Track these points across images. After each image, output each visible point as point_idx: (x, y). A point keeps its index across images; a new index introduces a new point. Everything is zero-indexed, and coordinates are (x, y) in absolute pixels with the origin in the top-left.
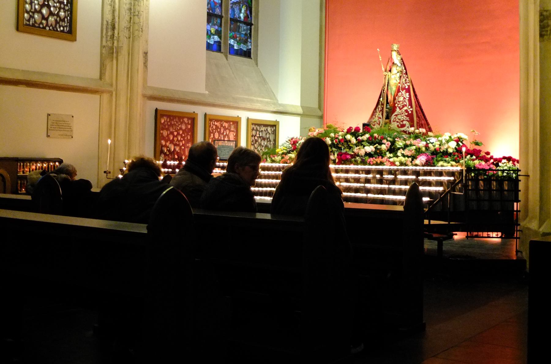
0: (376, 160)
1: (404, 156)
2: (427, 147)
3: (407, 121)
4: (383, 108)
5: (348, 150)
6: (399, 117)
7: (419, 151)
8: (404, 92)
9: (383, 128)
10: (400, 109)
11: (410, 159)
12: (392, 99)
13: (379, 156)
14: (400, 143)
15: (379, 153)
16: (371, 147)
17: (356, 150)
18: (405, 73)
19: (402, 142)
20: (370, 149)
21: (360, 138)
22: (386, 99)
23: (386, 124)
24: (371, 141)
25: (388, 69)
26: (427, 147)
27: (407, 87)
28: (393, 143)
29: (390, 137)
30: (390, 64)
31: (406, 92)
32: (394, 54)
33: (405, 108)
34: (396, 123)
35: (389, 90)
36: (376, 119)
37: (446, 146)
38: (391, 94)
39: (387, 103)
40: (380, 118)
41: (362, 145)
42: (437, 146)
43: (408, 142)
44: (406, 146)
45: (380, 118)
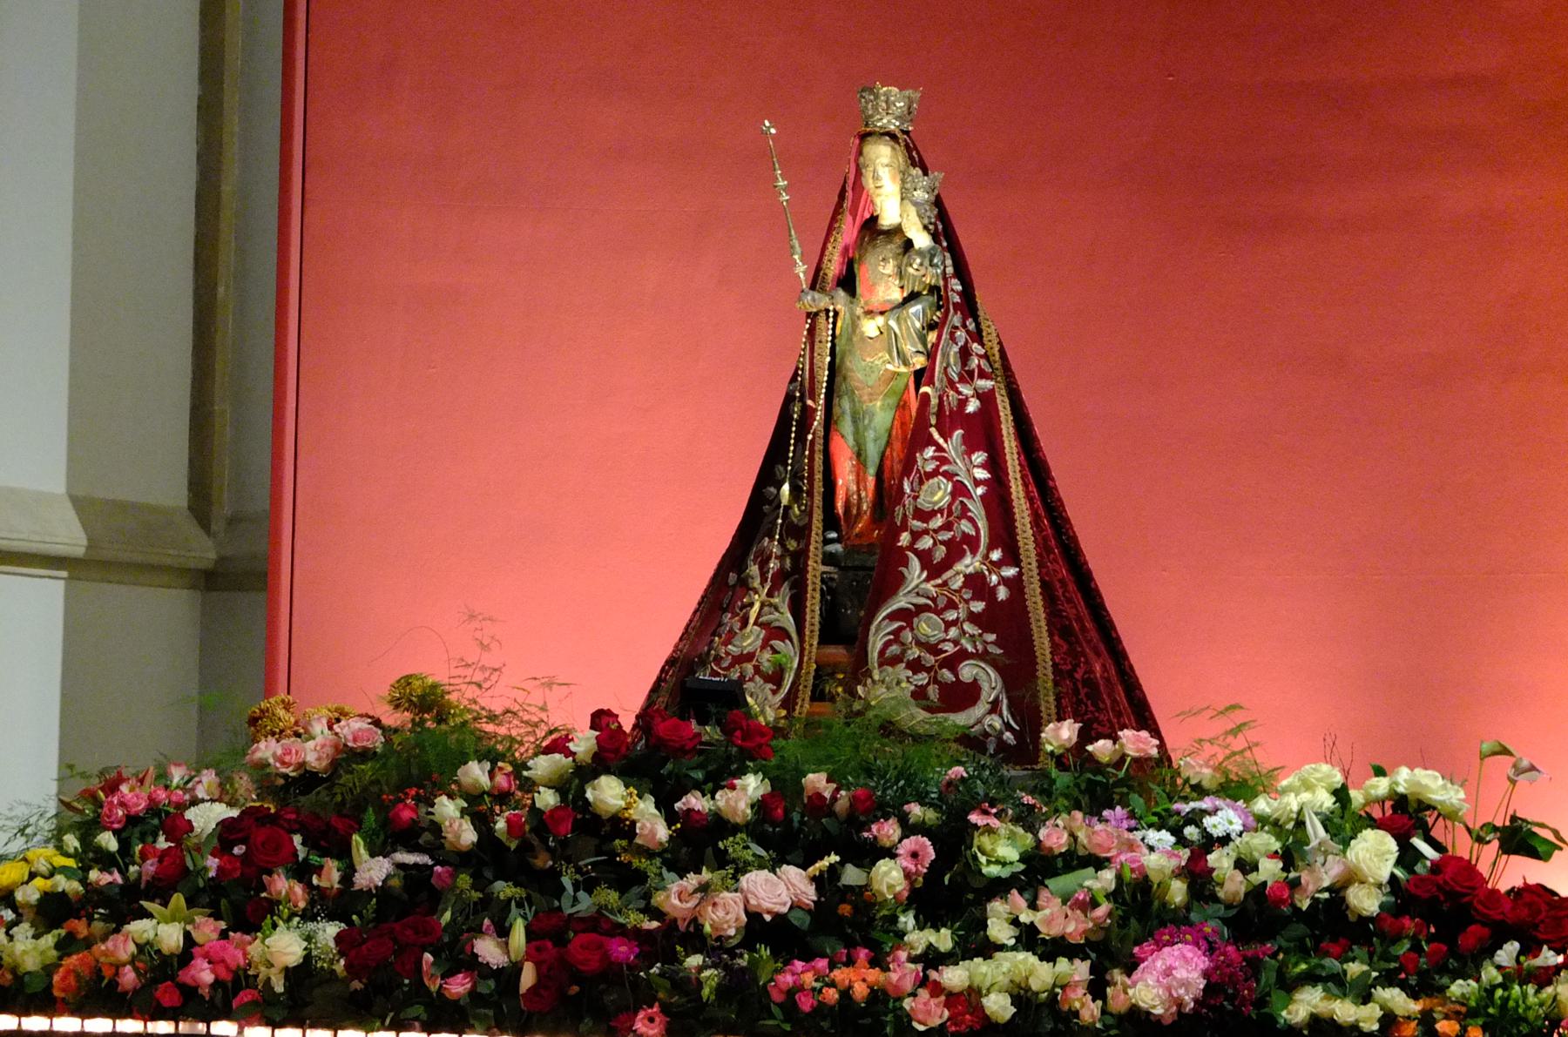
0: (839, 974)
1: (1028, 938)
2: (1198, 877)
3: (983, 656)
4: (800, 557)
5: (612, 897)
6: (928, 627)
7: (1140, 915)
8: (953, 446)
9: (804, 706)
10: (934, 569)
11: (1080, 970)
12: (868, 494)
13: (850, 944)
14: (1001, 849)
15: (846, 923)
16: (791, 872)
17: (676, 894)
18: (957, 300)
19: (1012, 837)
20: (780, 888)
21: (695, 801)
22: (819, 487)
23: (823, 672)
24: (785, 833)
25: (833, 268)
26: (1198, 877)
27: (972, 406)
28: (953, 839)
29: (922, 800)
30: (848, 231)
31: (970, 446)
32: (883, 160)
33: (969, 564)
34: (902, 671)
35: (846, 427)
36: (751, 639)
37: (1328, 873)
38: (860, 455)
39: (831, 521)
40: (782, 634)
41: (722, 860)
42: (1270, 870)
43: (1055, 836)
44: (1038, 869)
45: (782, 634)
